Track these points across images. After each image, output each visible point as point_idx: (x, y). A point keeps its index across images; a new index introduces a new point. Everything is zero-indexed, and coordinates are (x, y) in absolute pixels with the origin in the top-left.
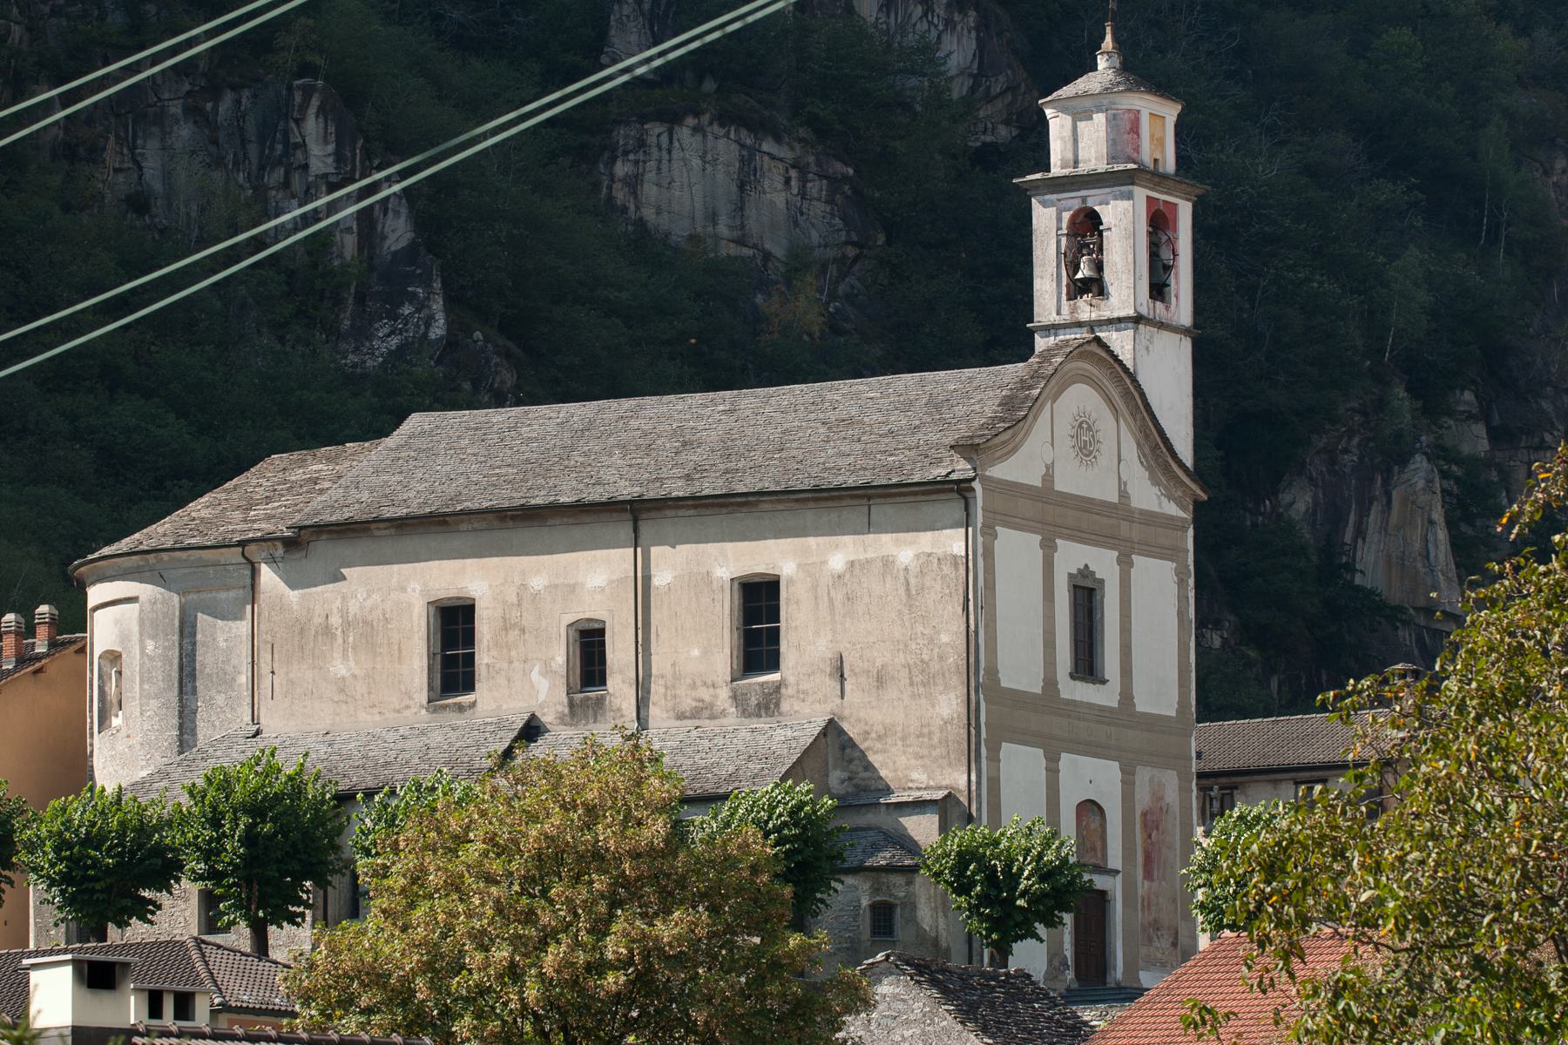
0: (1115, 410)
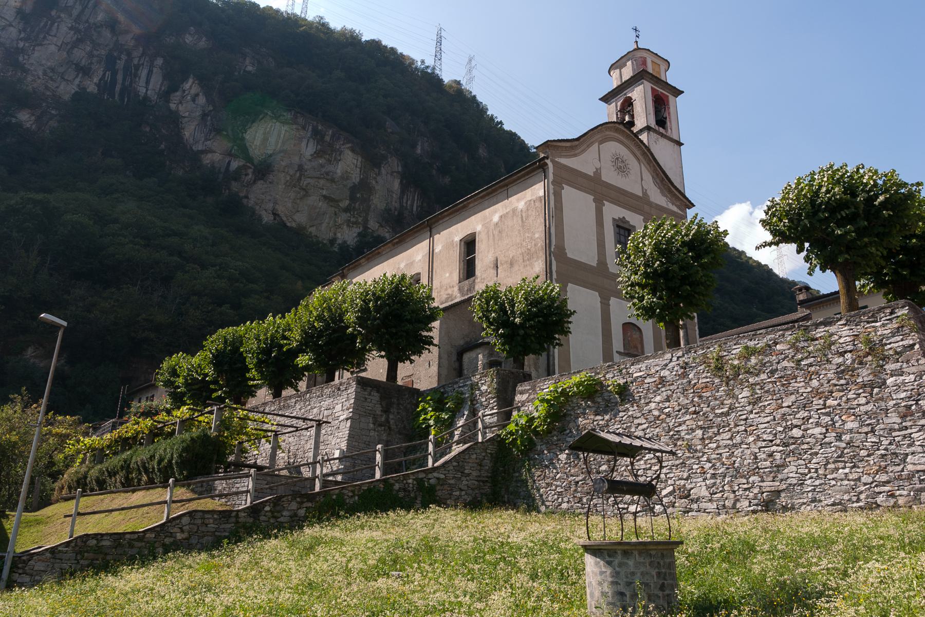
0: (638, 159)
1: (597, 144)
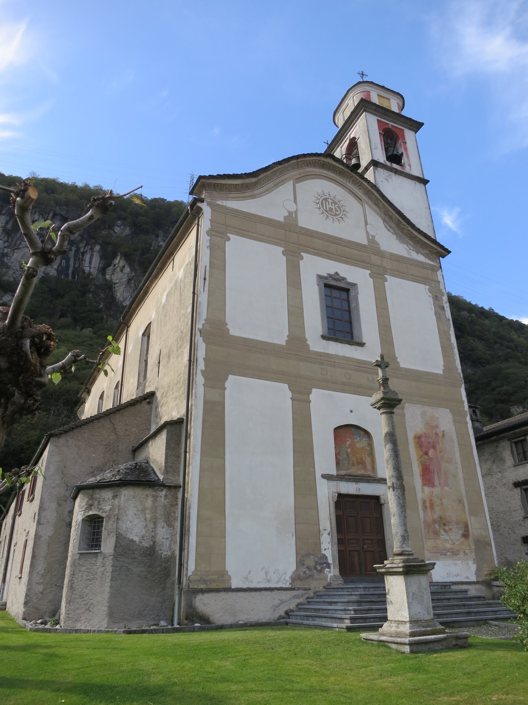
1: (291, 183)
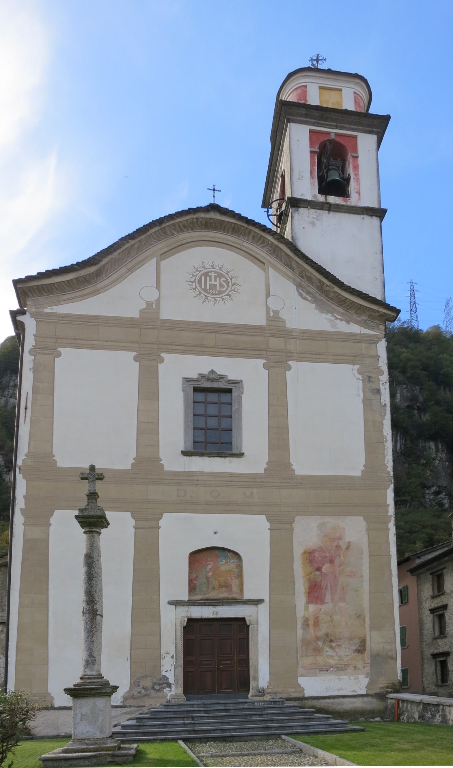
1: (154, 261)
